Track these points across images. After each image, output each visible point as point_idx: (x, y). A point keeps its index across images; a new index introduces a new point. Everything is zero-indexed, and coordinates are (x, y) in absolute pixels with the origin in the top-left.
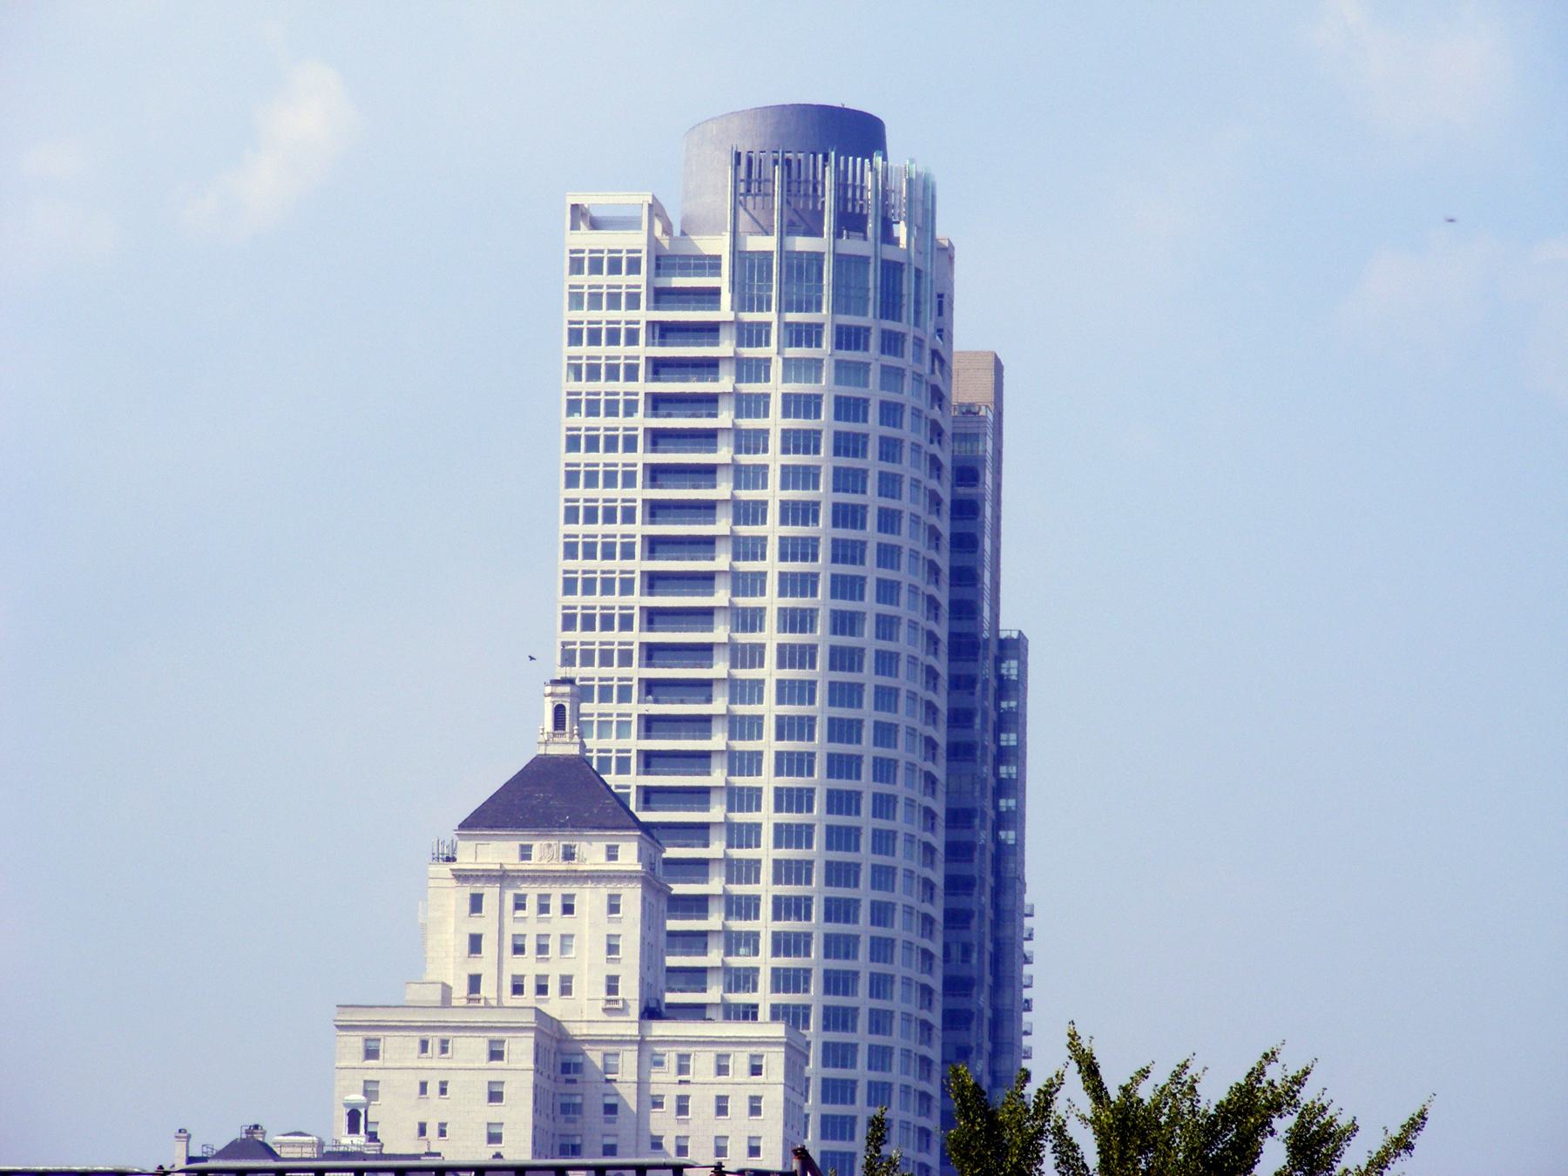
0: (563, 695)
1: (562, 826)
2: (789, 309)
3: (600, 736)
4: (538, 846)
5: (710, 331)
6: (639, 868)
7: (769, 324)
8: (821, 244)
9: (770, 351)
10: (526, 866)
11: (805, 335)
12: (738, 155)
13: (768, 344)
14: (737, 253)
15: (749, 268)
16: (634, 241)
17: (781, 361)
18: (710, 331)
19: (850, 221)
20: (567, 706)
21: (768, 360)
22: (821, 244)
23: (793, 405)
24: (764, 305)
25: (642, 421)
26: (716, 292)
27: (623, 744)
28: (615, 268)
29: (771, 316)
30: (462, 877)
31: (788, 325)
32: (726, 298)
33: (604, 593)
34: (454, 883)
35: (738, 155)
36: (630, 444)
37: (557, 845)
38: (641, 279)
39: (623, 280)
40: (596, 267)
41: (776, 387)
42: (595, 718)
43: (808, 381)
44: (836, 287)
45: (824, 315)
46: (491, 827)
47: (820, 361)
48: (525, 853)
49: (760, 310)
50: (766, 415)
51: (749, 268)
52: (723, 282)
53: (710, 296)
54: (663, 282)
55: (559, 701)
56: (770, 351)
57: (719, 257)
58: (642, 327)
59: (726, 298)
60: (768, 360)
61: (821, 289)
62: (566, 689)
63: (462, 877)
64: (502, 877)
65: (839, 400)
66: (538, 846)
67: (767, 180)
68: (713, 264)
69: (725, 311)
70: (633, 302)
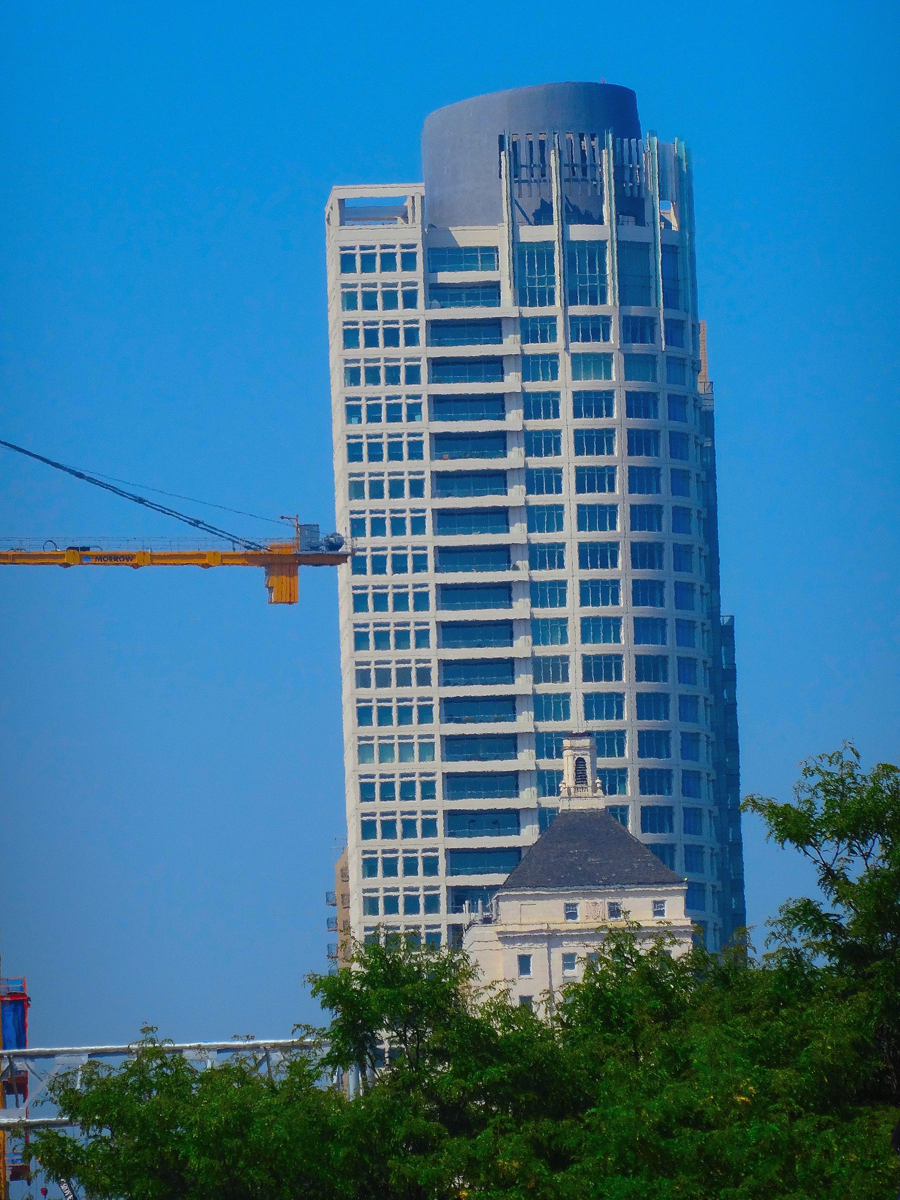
0: (584, 748)
1: (607, 883)
2: (573, 302)
3: (421, 759)
4: (583, 906)
5: (492, 329)
6: (688, 922)
7: (554, 319)
8: (549, 233)
9: (557, 346)
10: (571, 925)
11: (594, 329)
12: (501, 138)
13: (554, 339)
14: (517, 246)
15: (531, 259)
16: (408, 234)
17: (568, 359)
18: (492, 329)
19: (632, 206)
20: (587, 759)
21: (555, 356)
22: (549, 233)
23: (587, 403)
24: (547, 298)
25: (427, 426)
26: (496, 286)
27: (426, 766)
28: (388, 262)
29: (555, 309)
30: (506, 938)
31: (574, 318)
32: (507, 293)
33: (396, 608)
34: (500, 945)
35: (501, 138)
36: (416, 452)
37: (602, 905)
38: (417, 276)
39: (398, 276)
40: (368, 264)
41: (565, 384)
42: (415, 740)
43: (598, 377)
44: (622, 275)
45: (610, 306)
46: (534, 887)
47: (610, 356)
48: (571, 913)
49: (542, 304)
50: (556, 415)
51: (531, 259)
52: (502, 273)
53: (489, 293)
54: (444, 277)
55: (579, 754)
56: (557, 346)
57: (496, 249)
58: (422, 326)
59: (507, 293)
60: (555, 356)
61: (552, 281)
62: (586, 742)
63: (506, 938)
64: (552, 938)
65: (631, 397)
66: (583, 906)
67: (566, 165)
68: (488, 256)
69: (507, 306)
70: (410, 300)
